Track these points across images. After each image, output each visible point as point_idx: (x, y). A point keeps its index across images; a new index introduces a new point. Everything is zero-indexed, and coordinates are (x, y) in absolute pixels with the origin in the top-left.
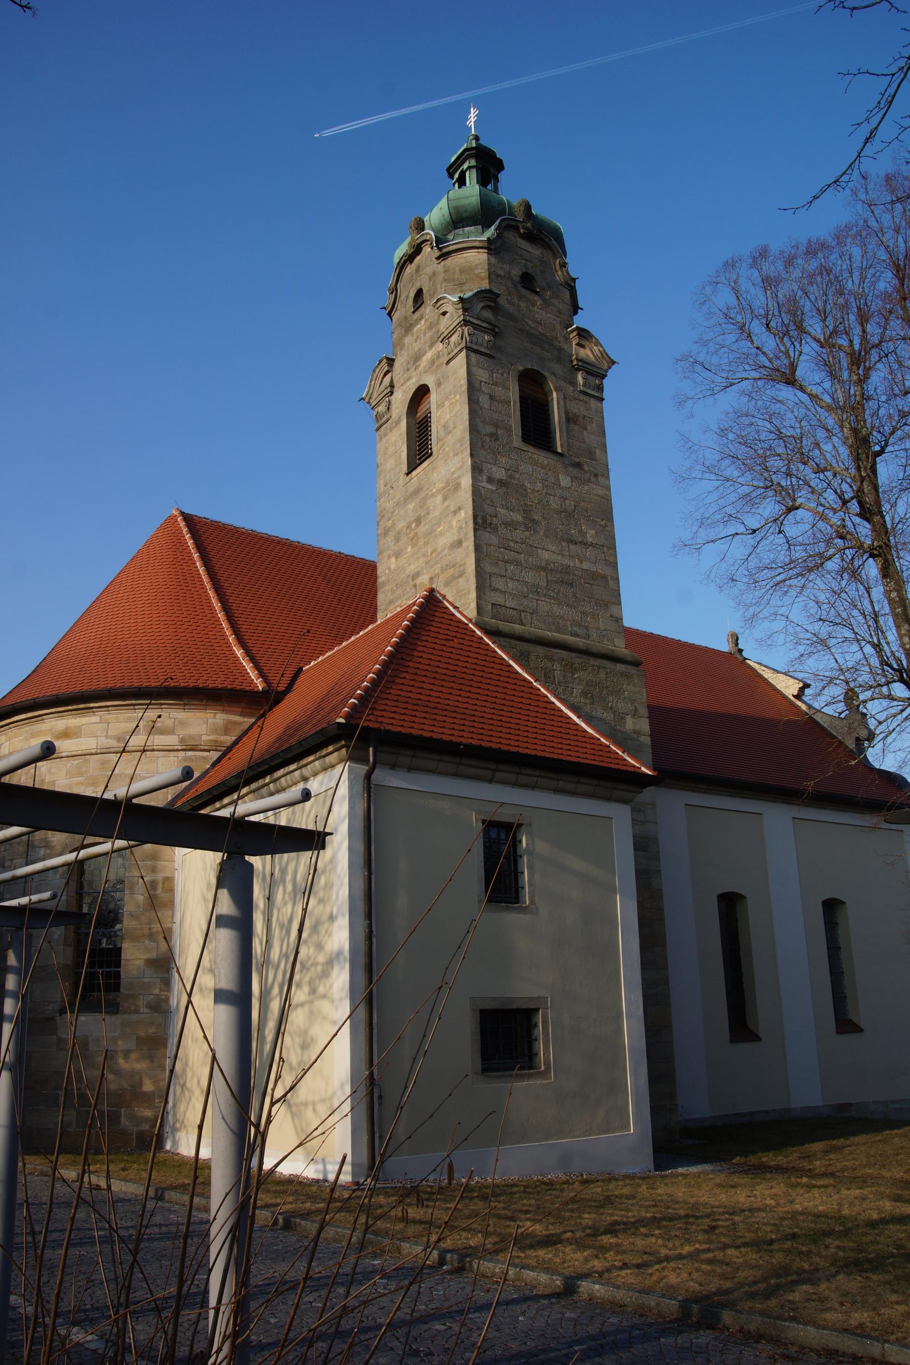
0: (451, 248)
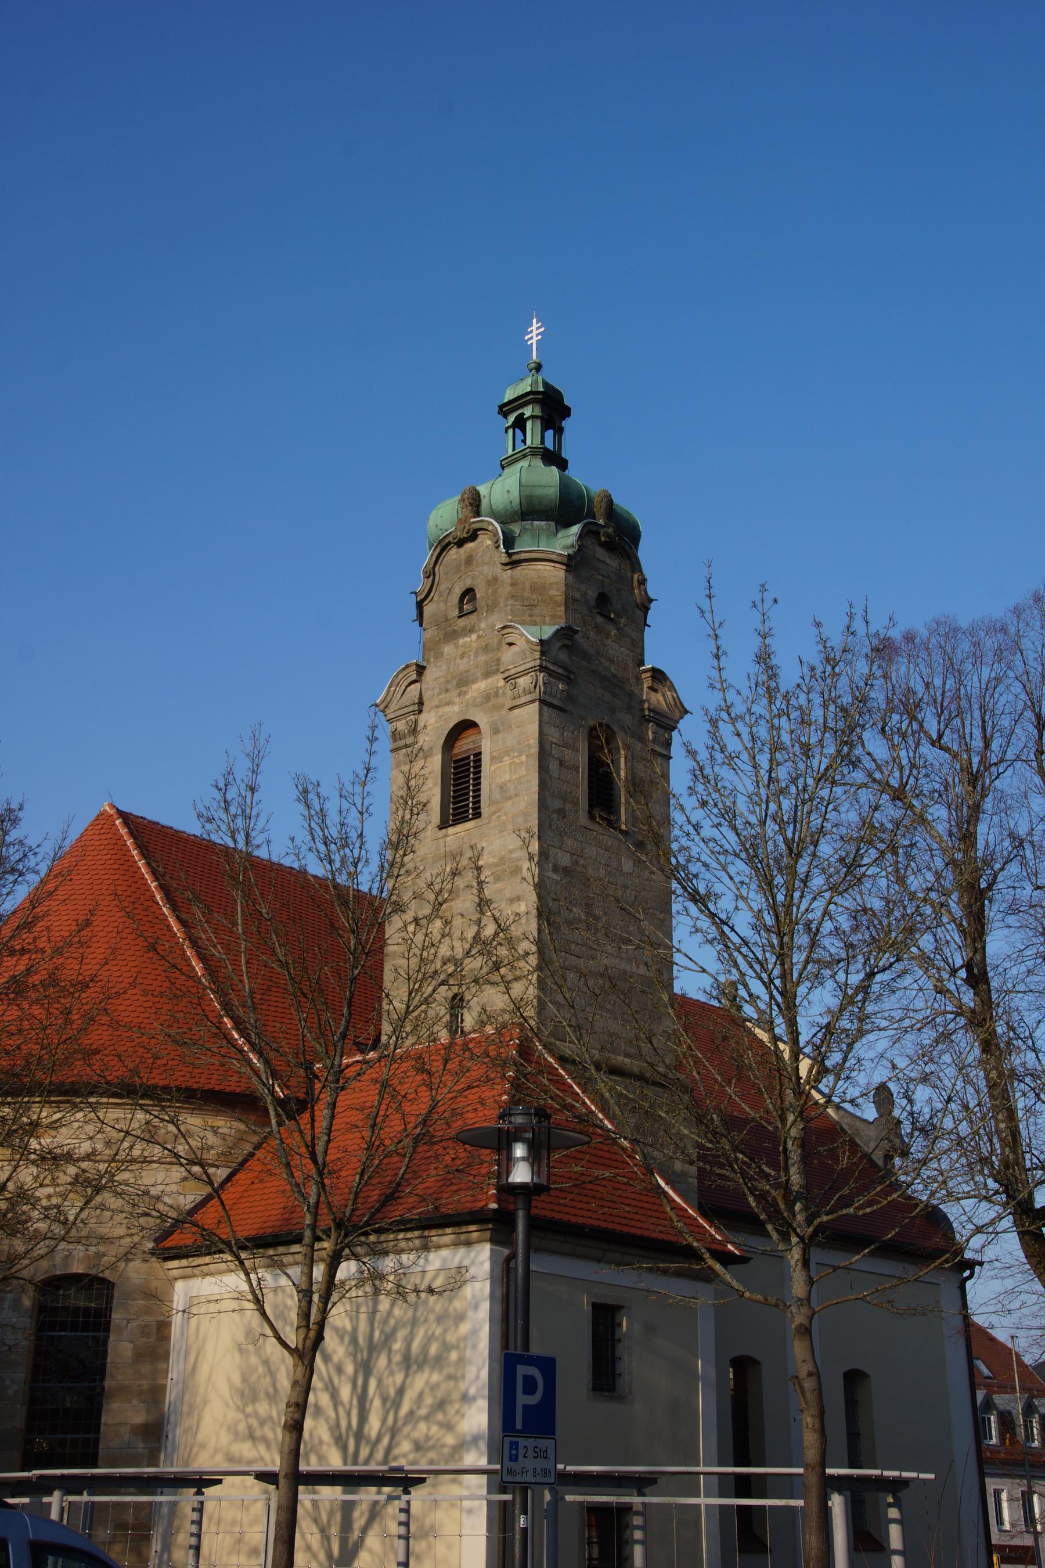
0: (523, 556)
